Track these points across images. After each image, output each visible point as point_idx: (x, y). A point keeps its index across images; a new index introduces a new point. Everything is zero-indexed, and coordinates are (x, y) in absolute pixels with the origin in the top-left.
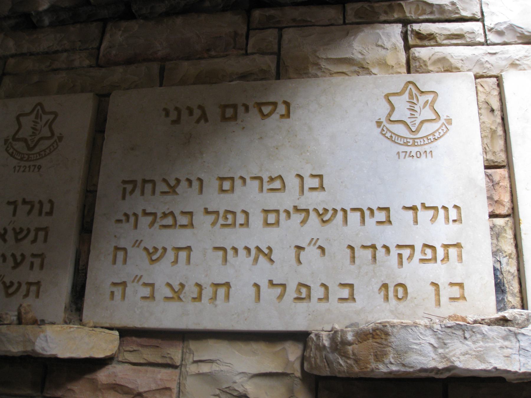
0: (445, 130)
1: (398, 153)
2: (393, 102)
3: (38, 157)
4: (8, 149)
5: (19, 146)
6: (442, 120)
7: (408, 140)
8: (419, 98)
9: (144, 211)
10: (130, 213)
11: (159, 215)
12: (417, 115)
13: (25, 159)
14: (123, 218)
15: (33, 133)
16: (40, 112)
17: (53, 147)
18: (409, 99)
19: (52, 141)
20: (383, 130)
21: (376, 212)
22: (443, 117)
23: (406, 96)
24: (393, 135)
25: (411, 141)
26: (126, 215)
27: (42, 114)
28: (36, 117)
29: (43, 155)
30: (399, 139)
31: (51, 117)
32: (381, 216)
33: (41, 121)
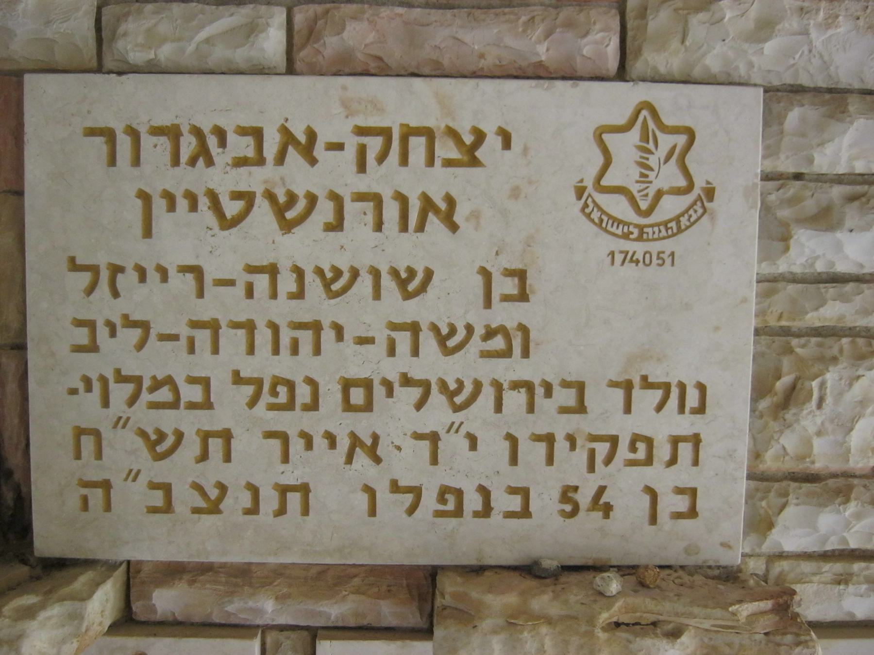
0: (700, 211)
1: (612, 254)
2: (611, 149)
3: (664, 233)
4: (587, 211)
5: (618, 207)
6: (697, 191)
7: (631, 229)
8: (661, 136)
9: (644, 378)
10: (94, 377)
11: (147, 383)
12: (652, 175)
13: (631, 236)
14: (81, 386)
15: (643, 175)
16: (651, 125)
17: (696, 211)
18: (641, 140)
19: (689, 198)
20: (586, 205)
21: (557, 390)
22: (699, 183)
23: (635, 135)
24: (603, 217)
25: (636, 232)
26: (88, 383)
27: (658, 133)
28: (645, 137)
29: (675, 231)
30: (615, 224)
31: (681, 140)
32: (568, 397)
33: (656, 147)
